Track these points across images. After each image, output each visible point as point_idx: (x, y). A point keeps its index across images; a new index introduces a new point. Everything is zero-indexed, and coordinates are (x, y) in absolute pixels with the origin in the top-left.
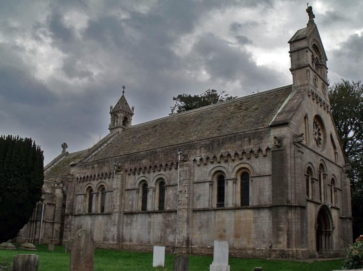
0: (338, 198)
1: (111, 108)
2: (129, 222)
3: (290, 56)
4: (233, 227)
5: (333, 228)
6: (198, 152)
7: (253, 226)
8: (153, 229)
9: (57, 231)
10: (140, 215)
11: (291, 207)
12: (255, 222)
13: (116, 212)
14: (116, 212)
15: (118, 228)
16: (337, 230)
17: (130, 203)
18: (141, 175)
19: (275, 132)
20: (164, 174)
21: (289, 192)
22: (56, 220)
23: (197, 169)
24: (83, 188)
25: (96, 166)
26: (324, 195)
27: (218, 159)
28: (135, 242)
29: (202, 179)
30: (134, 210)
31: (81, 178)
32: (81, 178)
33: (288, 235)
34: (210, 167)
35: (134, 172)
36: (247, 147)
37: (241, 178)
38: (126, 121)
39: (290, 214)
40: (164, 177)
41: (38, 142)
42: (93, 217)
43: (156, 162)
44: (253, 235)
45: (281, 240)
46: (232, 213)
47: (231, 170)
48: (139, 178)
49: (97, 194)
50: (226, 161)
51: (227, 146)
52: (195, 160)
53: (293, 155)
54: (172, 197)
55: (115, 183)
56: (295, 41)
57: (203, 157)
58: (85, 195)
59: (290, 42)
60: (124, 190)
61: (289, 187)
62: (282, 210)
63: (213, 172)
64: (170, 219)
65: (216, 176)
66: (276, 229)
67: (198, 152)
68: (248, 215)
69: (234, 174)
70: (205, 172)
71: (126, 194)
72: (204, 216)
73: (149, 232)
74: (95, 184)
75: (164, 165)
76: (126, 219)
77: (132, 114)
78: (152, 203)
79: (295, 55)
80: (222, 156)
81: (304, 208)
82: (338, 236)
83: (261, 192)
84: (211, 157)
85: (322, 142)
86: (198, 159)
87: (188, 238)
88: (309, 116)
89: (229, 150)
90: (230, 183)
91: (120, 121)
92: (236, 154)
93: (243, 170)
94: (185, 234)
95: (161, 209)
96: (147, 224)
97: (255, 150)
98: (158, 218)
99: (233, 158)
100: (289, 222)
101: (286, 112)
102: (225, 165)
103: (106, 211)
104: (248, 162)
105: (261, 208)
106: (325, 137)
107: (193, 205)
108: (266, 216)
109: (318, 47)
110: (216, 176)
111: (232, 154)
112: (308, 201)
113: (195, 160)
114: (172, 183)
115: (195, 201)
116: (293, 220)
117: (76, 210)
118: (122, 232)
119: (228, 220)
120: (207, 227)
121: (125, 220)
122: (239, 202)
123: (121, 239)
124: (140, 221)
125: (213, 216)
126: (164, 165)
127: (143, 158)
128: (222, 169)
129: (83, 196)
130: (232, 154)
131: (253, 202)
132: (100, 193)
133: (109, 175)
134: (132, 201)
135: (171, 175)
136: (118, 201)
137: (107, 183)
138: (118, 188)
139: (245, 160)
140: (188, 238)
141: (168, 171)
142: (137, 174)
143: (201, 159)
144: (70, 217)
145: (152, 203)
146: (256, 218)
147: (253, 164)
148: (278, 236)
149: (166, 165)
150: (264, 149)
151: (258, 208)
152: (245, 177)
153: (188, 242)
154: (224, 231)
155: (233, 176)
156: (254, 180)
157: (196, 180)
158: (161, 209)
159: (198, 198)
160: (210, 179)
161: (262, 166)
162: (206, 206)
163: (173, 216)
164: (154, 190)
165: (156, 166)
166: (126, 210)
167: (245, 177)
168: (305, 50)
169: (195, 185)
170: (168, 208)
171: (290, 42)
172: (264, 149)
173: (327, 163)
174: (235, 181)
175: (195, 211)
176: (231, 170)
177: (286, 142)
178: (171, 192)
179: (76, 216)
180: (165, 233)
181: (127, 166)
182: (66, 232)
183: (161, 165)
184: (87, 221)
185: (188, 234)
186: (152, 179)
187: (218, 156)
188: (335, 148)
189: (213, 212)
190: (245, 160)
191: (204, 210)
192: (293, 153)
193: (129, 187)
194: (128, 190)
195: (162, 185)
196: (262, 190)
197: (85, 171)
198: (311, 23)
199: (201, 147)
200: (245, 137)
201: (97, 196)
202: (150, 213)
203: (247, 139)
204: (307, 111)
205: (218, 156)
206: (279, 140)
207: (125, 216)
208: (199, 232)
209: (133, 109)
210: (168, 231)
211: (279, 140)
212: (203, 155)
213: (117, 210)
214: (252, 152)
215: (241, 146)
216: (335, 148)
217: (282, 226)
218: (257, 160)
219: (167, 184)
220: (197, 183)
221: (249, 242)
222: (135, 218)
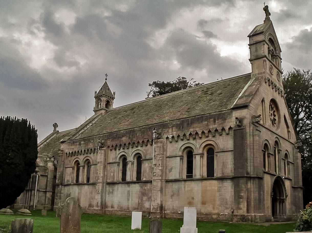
0: (291, 170)
1: (96, 92)
2: (111, 191)
3: (250, 48)
4: (200, 195)
5: (287, 196)
6: (170, 130)
7: (217, 194)
8: (132, 197)
9: (49, 199)
10: (120, 185)
11: (250, 178)
12: (219, 191)
13: (99, 183)
14: (99, 183)
15: (102, 196)
16: (290, 198)
17: (112, 174)
18: (122, 150)
19: (236, 114)
20: (141, 150)
21: (249, 165)
22: (48, 189)
23: (169, 145)
24: (73, 160)
25: (82, 143)
26: (279, 167)
27: (188, 137)
28: (116, 208)
29: (174, 154)
30: (115, 181)
31: (69, 153)
32: (69, 153)
33: (247, 202)
34: (181, 143)
35: (115, 148)
36: (212, 127)
37: (207, 153)
38: (108, 104)
39: (249, 184)
40: (141, 152)
41: (33, 123)
42: (80, 187)
43: (134, 139)
44: (218, 202)
45: (242, 206)
46: (199, 183)
47: (198, 146)
48: (119, 153)
49: (84, 167)
50: (194, 139)
51: (195, 125)
52: (167, 138)
53: (252, 133)
54: (147, 169)
55: (99, 157)
56: (253, 35)
57: (174, 135)
58: (73, 168)
59: (249, 36)
60: (107, 164)
61: (249, 161)
62: (242, 181)
63: (183, 148)
64: (146, 188)
65: (185, 151)
66: (237, 197)
67: (170, 130)
68: (213, 185)
69: (201, 149)
70: (176, 148)
71: (108, 167)
72: (175, 186)
73: (128, 200)
74: (81, 158)
75: (141, 142)
76: (108, 188)
77: (113, 98)
78: (131, 175)
79: (254, 47)
80: (190, 134)
81: (261, 179)
82: (291, 203)
83: (224, 165)
84: (181, 135)
85: (276, 122)
86: (170, 136)
87: (162, 205)
88: (266, 100)
89: (197, 129)
90: (198, 157)
91: (103, 104)
92: (203, 132)
93: (209, 147)
94: (159, 201)
95: (139, 180)
96: (126, 192)
97: (219, 129)
98: (136, 188)
99: (200, 136)
100: (248, 191)
101: (246, 96)
102: (193, 142)
103: (91, 181)
104: (213, 139)
105: (224, 179)
106: (279, 118)
107: (166, 176)
108: (228, 186)
109: (274, 40)
110: (206, 149)
111: (200, 133)
112: (265, 172)
113: (167, 138)
114: (148, 157)
115: (168, 173)
116: (252, 189)
117: (66, 181)
118: (105, 200)
119: (196, 189)
120: (178, 195)
121: (108, 189)
122: (205, 174)
123: (104, 205)
124: (120, 190)
125: (183, 186)
126: (141, 142)
127: (123, 136)
128: (191, 146)
129: (71, 169)
130: (200, 133)
131: (217, 174)
132: (86, 166)
133: (93, 151)
134: (114, 173)
135: (147, 151)
136: (102, 173)
137: (92, 157)
138: (101, 162)
139: (210, 138)
140: (162, 205)
141: (144, 147)
142: (117, 150)
143: (173, 137)
144: (60, 186)
145: (131, 175)
146: (220, 187)
147: (218, 141)
148: (239, 203)
149: (143, 142)
150: (227, 129)
151: (222, 179)
152: (211, 152)
153: (162, 208)
154: (193, 198)
155: (200, 151)
156: (218, 154)
157: (168, 155)
158: (139, 180)
159: (171, 170)
160: (180, 154)
161: (225, 142)
162: (177, 177)
163: (149, 185)
164: (133, 164)
165: (134, 143)
166: (108, 181)
167: (211, 152)
168: (262, 43)
169: (168, 159)
170: (144, 179)
171: (249, 36)
172: (227, 129)
173: (281, 141)
174: (202, 155)
175: (168, 181)
176: (198, 146)
177: (246, 122)
178: (147, 165)
179: (65, 185)
180: (142, 200)
181: (109, 143)
182: (57, 199)
183: (138, 142)
184: (75, 191)
185: (162, 201)
186: (130, 154)
187: (188, 134)
188: (288, 127)
189: (183, 183)
190: (210, 138)
191: (176, 181)
192: (252, 131)
193: (111, 161)
194: (110, 163)
195: (139, 159)
196: (225, 163)
197: (73, 147)
198: (267, 20)
199: (173, 127)
200: (210, 118)
201: (84, 168)
202: (129, 183)
203: (212, 120)
204: (264, 95)
205: (188, 134)
206: (240, 120)
207: (108, 186)
208: (171, 200)
209: (114, 93)
210: (145, 198)
211: (240, 120)
212: (175, 134)
213: (100, 180)
214: (216, 130)
215: (207, 125)
216: (288, 127)
217: (242, 194)
218: (221, 137)
219: (143, 158)
220: (169, 157)
221: (214, 208)
222: (116, 187)
